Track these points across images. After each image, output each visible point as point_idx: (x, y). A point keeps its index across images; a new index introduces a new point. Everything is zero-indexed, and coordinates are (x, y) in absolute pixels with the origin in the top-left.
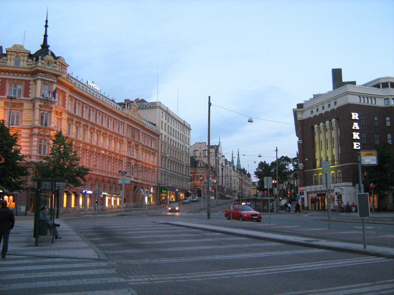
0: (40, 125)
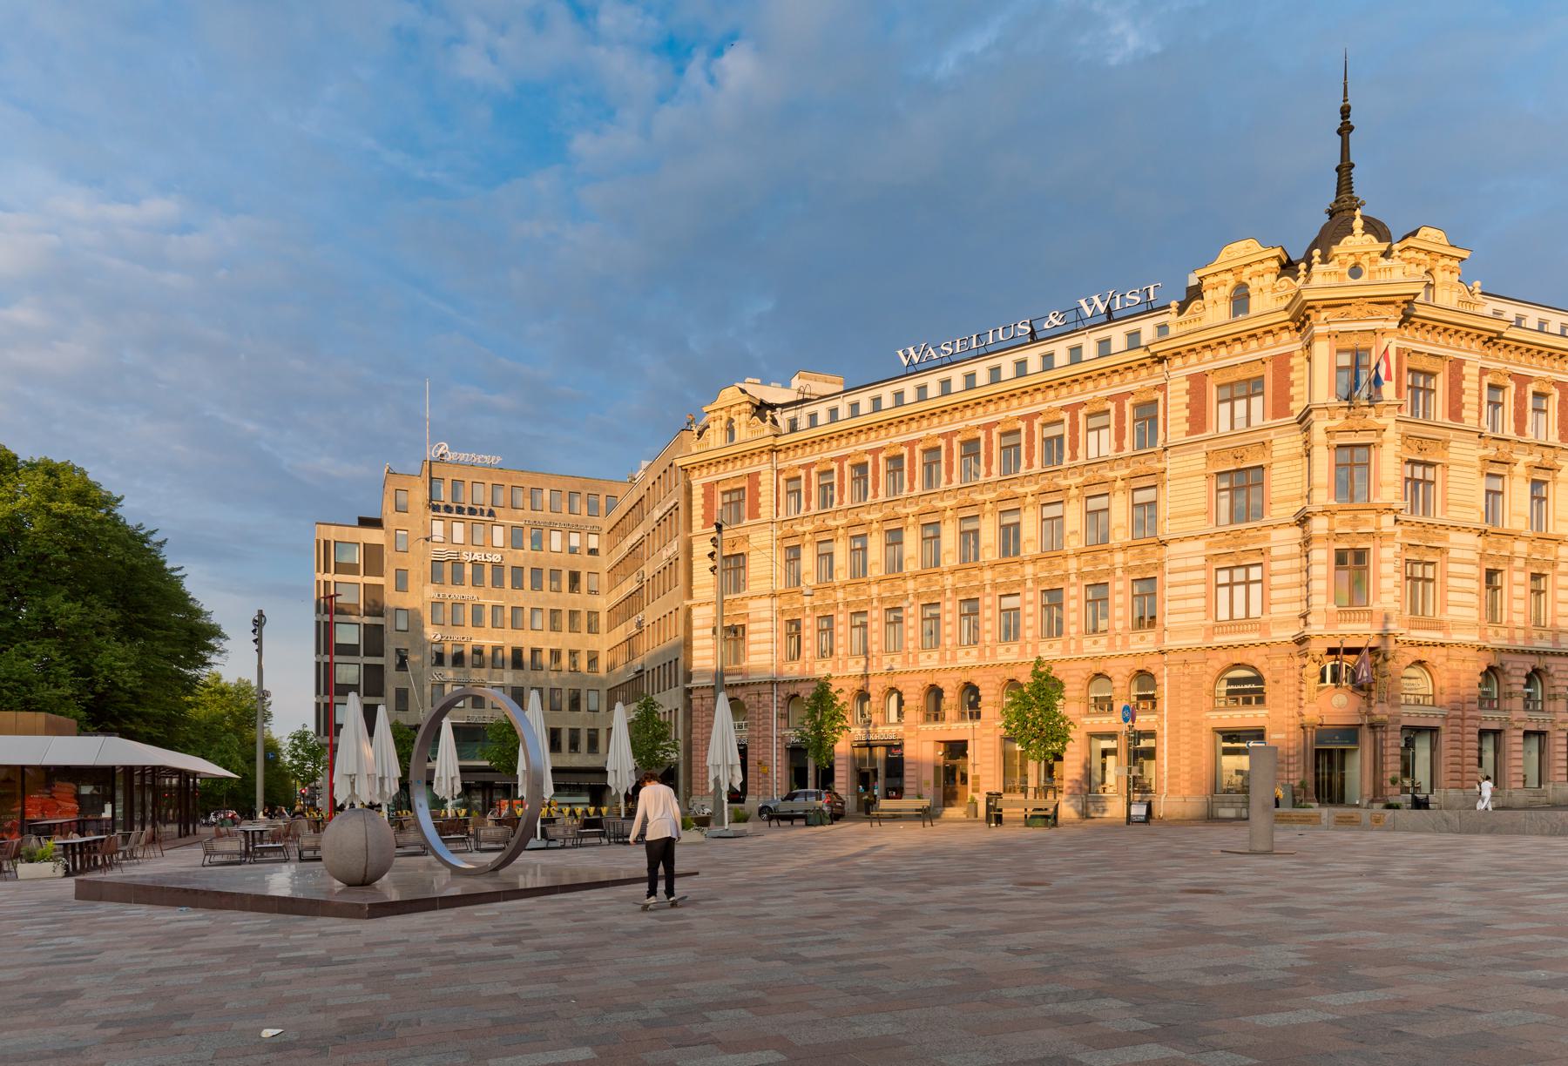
0: (1332, 502)
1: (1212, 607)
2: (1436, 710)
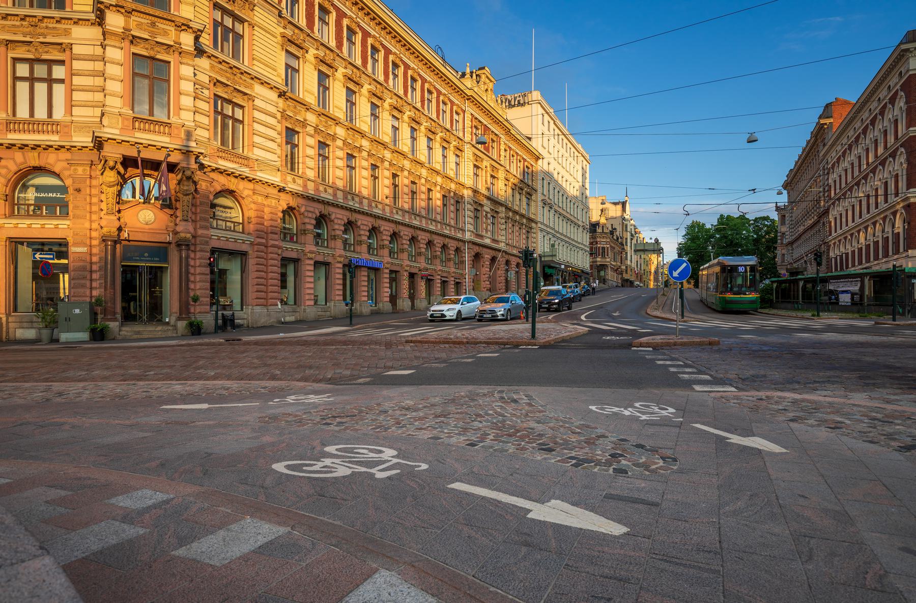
2: (244, 237)
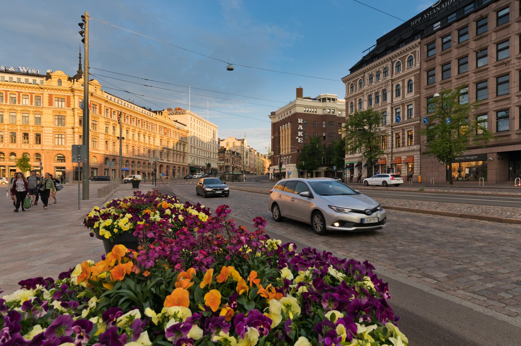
1: (54, 142)
